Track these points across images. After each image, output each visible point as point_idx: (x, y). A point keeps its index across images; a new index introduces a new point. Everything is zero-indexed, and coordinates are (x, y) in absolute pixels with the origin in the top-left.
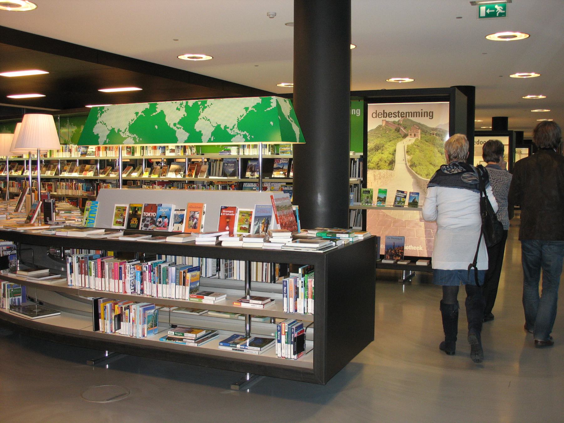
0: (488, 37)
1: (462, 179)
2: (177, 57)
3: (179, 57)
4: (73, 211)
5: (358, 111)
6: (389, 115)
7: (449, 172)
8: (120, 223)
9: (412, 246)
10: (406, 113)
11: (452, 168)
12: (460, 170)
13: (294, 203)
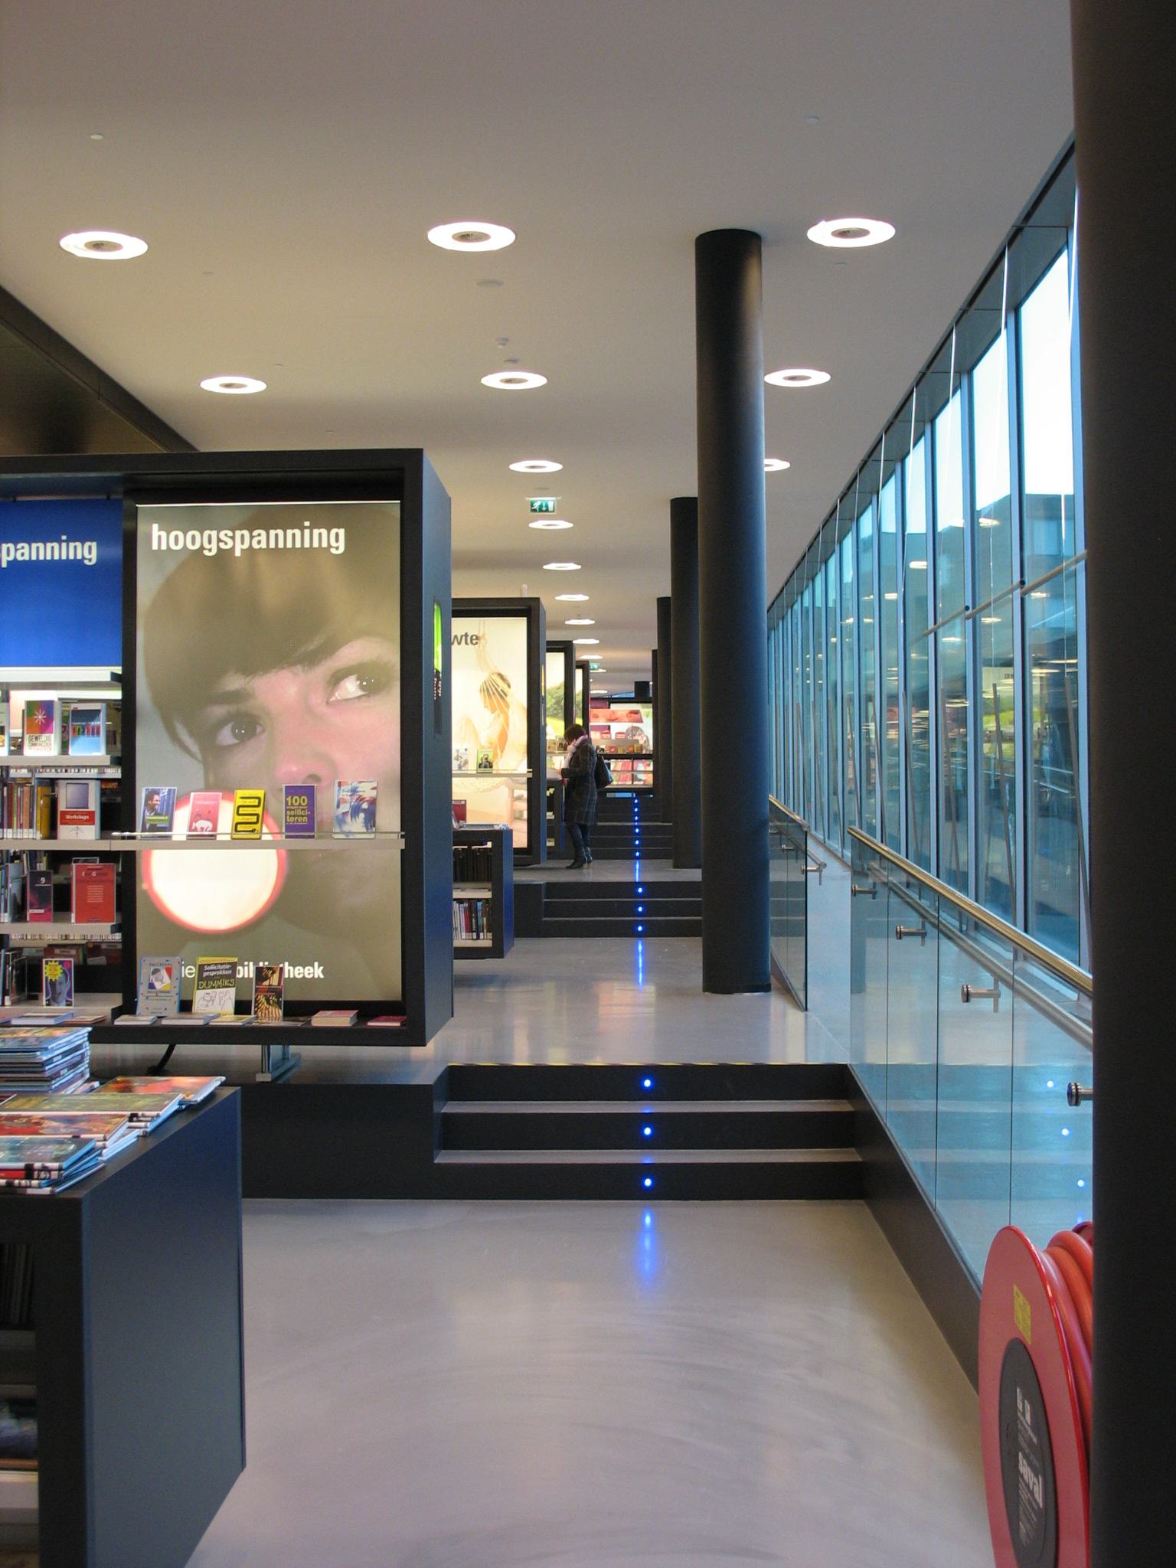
5: (337, 535)
6: (472, 640)
9: (289, 965)
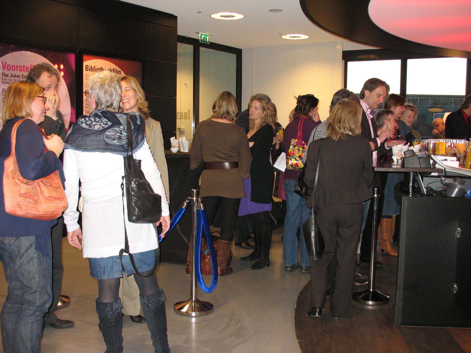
0: (308, 37)
1: (106, 139)
2: (210, 16)
3: (243, 16)
4: (221, 112)
7: (88, 127)
8: (287, 163)
11: (93, 121)
12: (104, 124)
13: (179, 151)
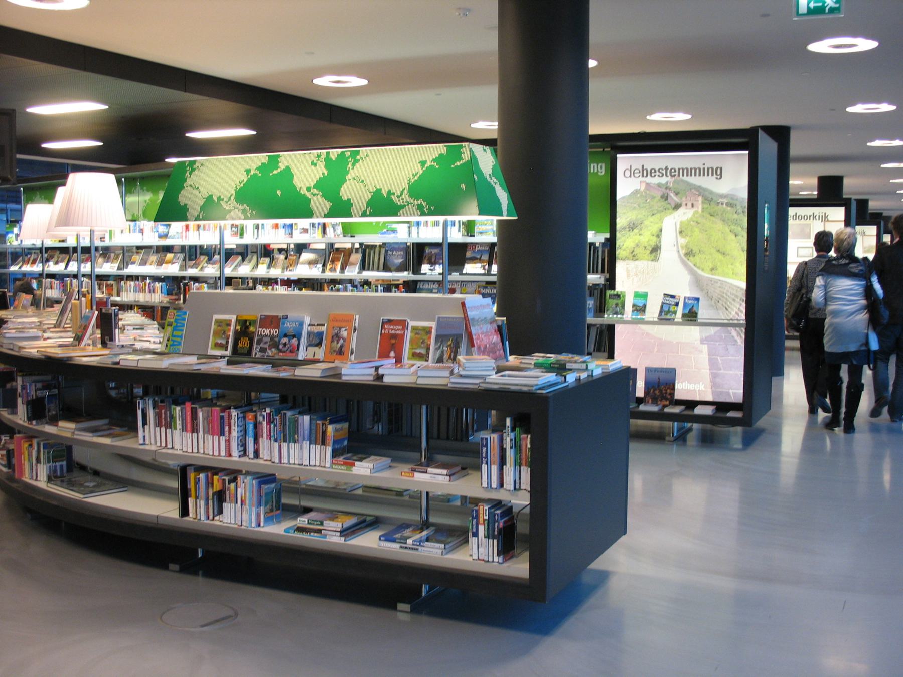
10: (679, 170)
